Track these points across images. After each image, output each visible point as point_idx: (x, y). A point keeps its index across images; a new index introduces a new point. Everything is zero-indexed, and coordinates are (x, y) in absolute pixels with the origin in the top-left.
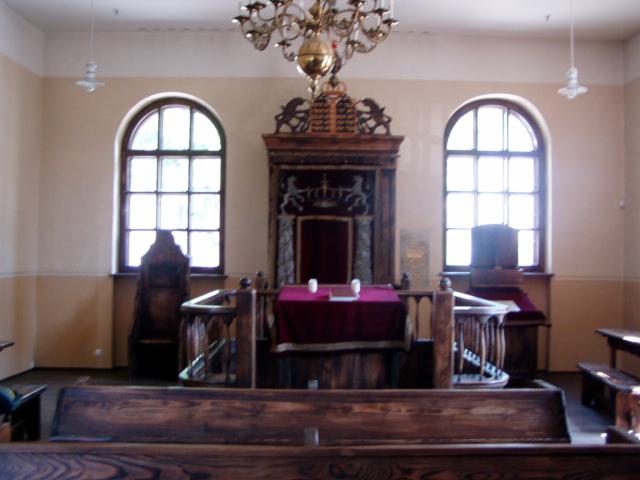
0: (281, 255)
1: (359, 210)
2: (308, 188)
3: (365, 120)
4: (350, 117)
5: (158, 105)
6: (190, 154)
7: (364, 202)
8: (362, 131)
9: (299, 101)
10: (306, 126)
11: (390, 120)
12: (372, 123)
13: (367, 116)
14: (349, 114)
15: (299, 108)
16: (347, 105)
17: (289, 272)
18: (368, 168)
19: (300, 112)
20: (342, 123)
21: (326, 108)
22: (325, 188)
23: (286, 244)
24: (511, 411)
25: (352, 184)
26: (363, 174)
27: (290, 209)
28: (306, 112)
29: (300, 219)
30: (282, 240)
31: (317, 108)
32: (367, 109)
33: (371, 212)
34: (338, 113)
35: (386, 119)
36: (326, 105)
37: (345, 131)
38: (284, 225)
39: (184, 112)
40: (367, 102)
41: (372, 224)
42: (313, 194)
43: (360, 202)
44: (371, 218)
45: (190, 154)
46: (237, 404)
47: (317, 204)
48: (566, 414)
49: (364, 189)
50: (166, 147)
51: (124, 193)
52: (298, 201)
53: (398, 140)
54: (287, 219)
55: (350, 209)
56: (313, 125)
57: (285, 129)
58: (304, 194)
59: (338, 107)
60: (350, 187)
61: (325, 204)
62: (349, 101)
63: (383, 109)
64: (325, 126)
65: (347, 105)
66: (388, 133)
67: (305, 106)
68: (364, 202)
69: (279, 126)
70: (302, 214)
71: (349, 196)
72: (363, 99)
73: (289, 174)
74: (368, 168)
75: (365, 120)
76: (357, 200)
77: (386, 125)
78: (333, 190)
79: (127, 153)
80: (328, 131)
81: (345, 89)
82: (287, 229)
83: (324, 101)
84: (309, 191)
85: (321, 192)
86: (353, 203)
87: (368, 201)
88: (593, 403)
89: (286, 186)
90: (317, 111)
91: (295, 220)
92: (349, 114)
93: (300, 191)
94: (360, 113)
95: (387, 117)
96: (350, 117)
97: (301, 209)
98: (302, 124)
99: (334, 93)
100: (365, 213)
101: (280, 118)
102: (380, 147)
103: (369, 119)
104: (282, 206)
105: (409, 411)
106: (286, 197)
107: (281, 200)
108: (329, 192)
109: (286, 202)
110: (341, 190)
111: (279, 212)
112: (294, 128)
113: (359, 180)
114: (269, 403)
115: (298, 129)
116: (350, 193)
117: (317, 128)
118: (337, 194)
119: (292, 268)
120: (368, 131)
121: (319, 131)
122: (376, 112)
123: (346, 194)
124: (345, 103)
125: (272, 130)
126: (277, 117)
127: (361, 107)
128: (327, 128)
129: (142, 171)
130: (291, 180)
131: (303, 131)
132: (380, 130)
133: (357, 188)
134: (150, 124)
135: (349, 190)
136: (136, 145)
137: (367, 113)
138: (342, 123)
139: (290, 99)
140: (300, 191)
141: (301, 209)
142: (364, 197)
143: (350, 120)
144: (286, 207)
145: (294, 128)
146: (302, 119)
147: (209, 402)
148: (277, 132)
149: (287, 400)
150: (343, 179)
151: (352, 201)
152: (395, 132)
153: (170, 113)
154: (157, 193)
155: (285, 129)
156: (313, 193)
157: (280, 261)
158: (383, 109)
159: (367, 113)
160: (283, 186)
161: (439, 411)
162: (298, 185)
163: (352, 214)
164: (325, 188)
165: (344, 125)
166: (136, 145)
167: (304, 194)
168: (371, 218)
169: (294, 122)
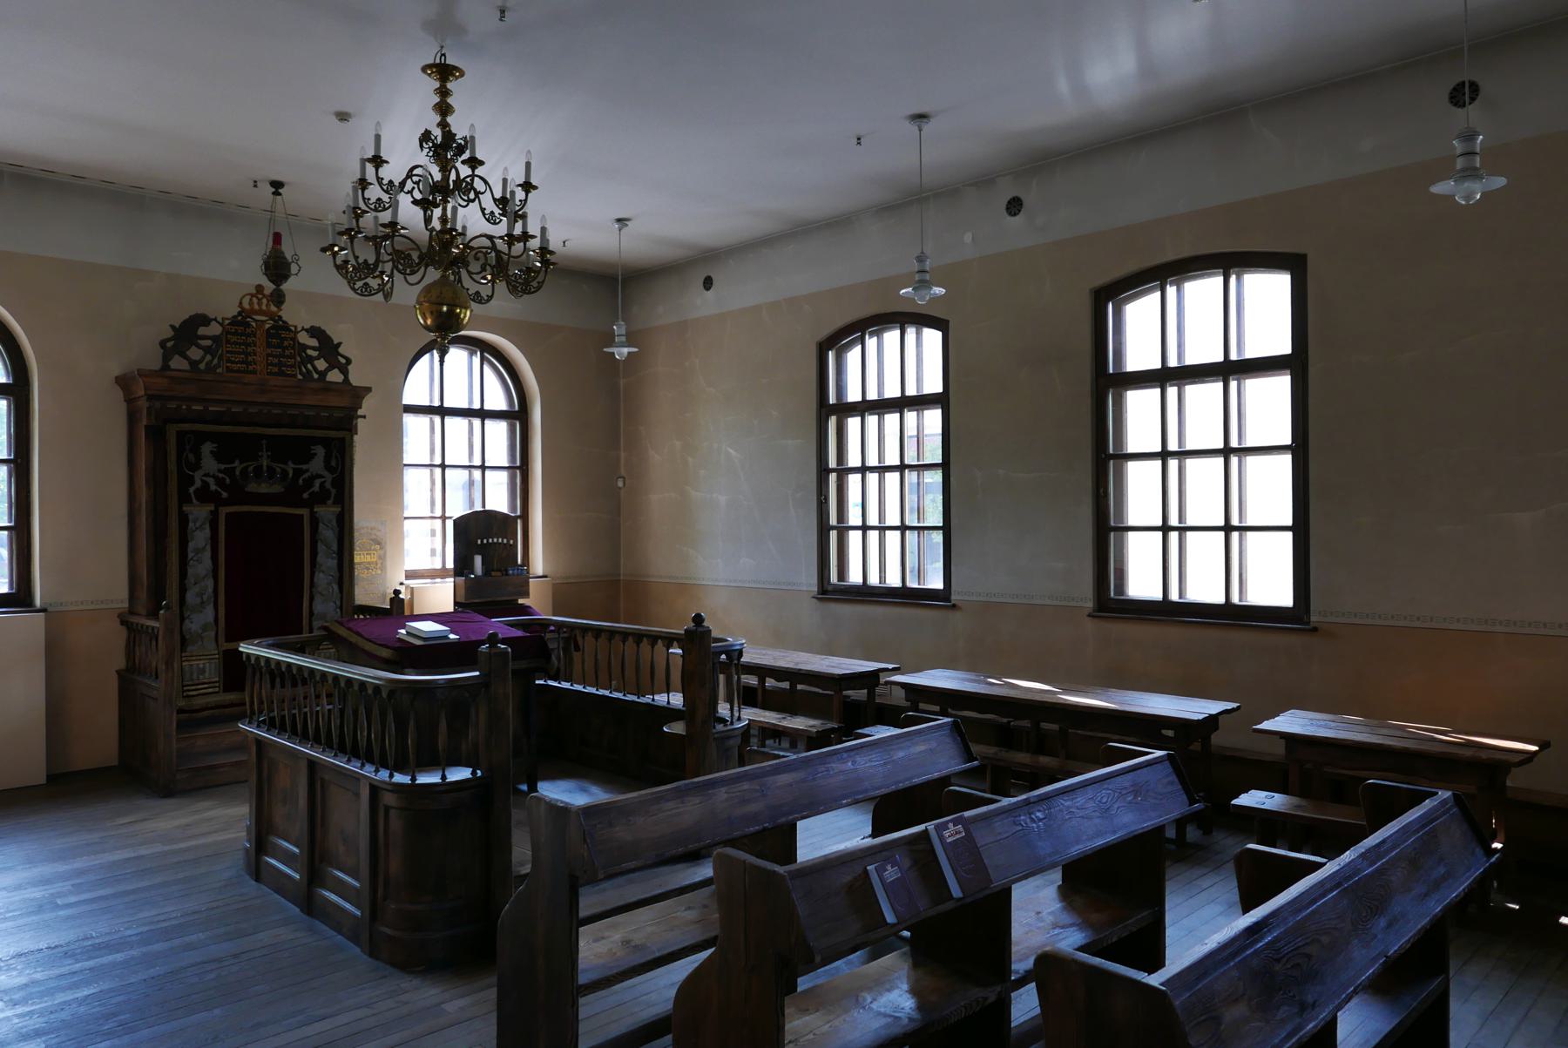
2: (237, 463)
3: (311, 359)
4: (287, 353)
7: (328, 485)
10: (215, 361)
11: (349, 361)
12: (321, 365)
14: (287, 348)
15: (202, 331)
17: (205, 597)
18: (332, 434)
20: (276, 361)
21: (248, 336)
26: (325, 442)
27: (205, 495)
28: (215, 339)
29: (224, 511)
31: (233, 334)
32: (314, 342)
34: (269, 345)
37: (281, 373)
40: (315, 332)
42: (244, 472)
43: (322, 485)
44: (337, 509)
46: (746, 786)
47: (252, 487)
49: (328, 467)
52: (220, 482)
53: (360, 393)
54: (199, 513)
55: (305, 496)
56: (228, 361)
57: (177, 363)
60: (307, 463)
61: (264, 488)
63: (339, 344)
67: (215, 329)
68: (328, 485)
69: (166, 358)
70: (227, 503)
71: (306, 476)
72: (307, 326)
73: (203, 437)
74: (332, 434)
76: (317, 483)
77: (344, 371)
78: (278, 467)
82: (201, 528)
84: (237, 466)
85: (258, 470)
86: (311, 486)
87: (333, 484)
88: (524, 787)
89: (199, 458)
90: (234, 339)
91: (215, 514)
92: (287, 348)
93: (223, 467)
94: (304, 347)
96: (287, 353)
97: (225, 495)
100: (330, 502)
101: (169, 344)
102: (335, 401)
104: (192, 490)
108: (271, 470)
109: (198, 484)
110: (290, 468)
113: (320, 451)
114: (771, 779)
115: (202, 366)
116: (307, 471)
118: (285, 473)
119: (210, 590)
121: (238, 371)
122: (329, 348)
123: (298, 473)
124: (281, 331)
126: (163, 344)
127: (304, 338)
128: (251, 368)
131: (210, 368)
132: (335, 376)
133: (317, 465)
135: (304, 467)
137: (313, 348)
138: (276, 361)
139: (714, 283)
140: (223, 467)
141: (225, 495)
142: (329, 477)
143: (288, 357)
146: (207, 350)
147: (723, 789)
148: (165, 367)
149: (784, 772)
150: (300, 451)
151: (309, 483)
157: (191, 580)
158: (339, 344)
159: (313, 348)
162: (217, 455)
163: (309, 504)
165: (280, 364)
168: (337, 509)
169: (195, 354)
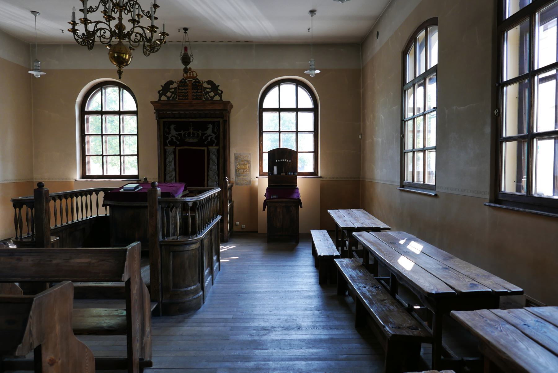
0: (167, 169)
1: (211, 143)
3: (208, 93)
4: (199, 91)
5: (278, 83)
6: (297, 110)
8: (207, 99)
9: (171, 82)
11: (222, 92)
12: (212, 94)
13: (209, 90)
14: (199, 89)
15: (171, 86)
16: (198, 84)
19: (172, 89)
21: (185, 86)
22: (191, 131)
23: (170, 162)
24: (93, 261)
25: (207, 128)
26: (213, 123)
27: (172, 143)
28: (175, 89)
29: (178, 148)
30: (168, 160)
32: (209, 86)
33: (218, 144)
34: (193, 89)
35: (220, 92)
36: (186, 84)
37: (197, 99)
38: (169, 152)
39: (292, 87)
40: (210, 82)
41: (218, 151)
45: (297, 110)
47: (187, 140)
48: (370, 260)
49: (213, 132)
50: (300, 106)
51: (83, 135)
52: (176, 138)
54: (170, 149)
55: (206, 143)
57: (164, 98)
58: (179, 135)
59: (193, 85)
61: (191, 140)
62: (199, 82)
63: (218, 86)
64: (186, 96)
65: (198, 84)
66: (221, 100)
67: (175, 85)
69: (160, 97)
75: (208, 93)
76: (210, 138)
77: (220, 96)
79: (83, 113)
80: (187, 99)
81: (197, 76)
83: (186, 82)
85: (189, 134)
91: (175, 149)
92: (199, 89)
93: (177, 133)
94: (206, 88)
95: (220, 90)
96: (199, 91)
98: (173, 95)
99: (190, 77)
100: (214, 145)
101: (161, 92)
103: (210, 92)
104: (167, 141)
105: (32, 260)
106: (170, 136)
107: (166, 138)
108: (193, 134)
109: (170, 139)
111: (165, 144)
112: (168, 98)
116: (206, 134)
117: (181, 98)
118: (198, 134)
119: (174, 176)
120: (210, 99)
121: (182, 99)
122: (215, 87)
124: (197, 83)
125: (156, 99)
126: (159, 92)
127: (205, 85)
129: (93, 123)
130: (173, 127)
132: (217, 98)
133: (209, 132)
134: (274, 92)
136: (265, 106)
137: (209, 88)
141: (178, 143)
144: (169, 142)
145: (168, 98)
146: (172, 93)
148: (160, 100)
151: (207, 138)
152: (225, 98)
153: (284, 87)
154: (120, 135)
155: (164, 98)
156: (185, 134)
158: (218, 86)
159: (209, 88)
160: (167, 130)
161: (52, 261)
162: (176, 129)
163: (207, 146)
164: (191, 131)
166: (265, 106)
167: (180, 135)
169: (169, 94)
